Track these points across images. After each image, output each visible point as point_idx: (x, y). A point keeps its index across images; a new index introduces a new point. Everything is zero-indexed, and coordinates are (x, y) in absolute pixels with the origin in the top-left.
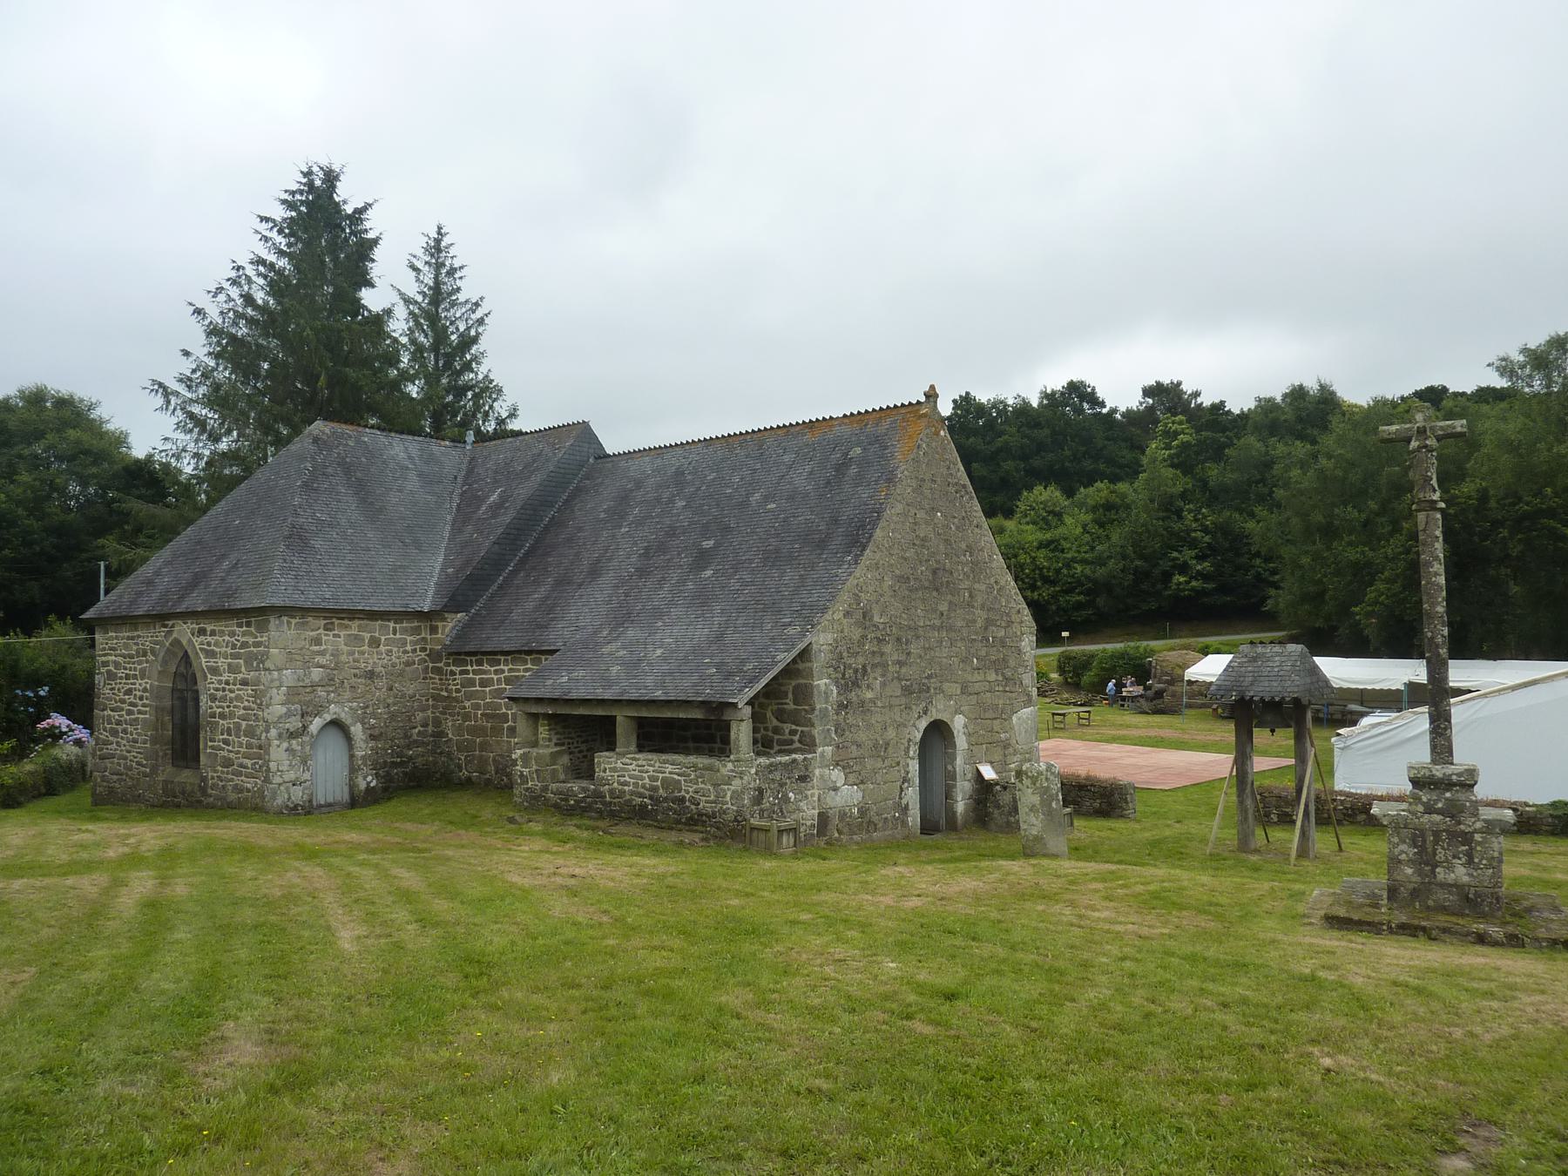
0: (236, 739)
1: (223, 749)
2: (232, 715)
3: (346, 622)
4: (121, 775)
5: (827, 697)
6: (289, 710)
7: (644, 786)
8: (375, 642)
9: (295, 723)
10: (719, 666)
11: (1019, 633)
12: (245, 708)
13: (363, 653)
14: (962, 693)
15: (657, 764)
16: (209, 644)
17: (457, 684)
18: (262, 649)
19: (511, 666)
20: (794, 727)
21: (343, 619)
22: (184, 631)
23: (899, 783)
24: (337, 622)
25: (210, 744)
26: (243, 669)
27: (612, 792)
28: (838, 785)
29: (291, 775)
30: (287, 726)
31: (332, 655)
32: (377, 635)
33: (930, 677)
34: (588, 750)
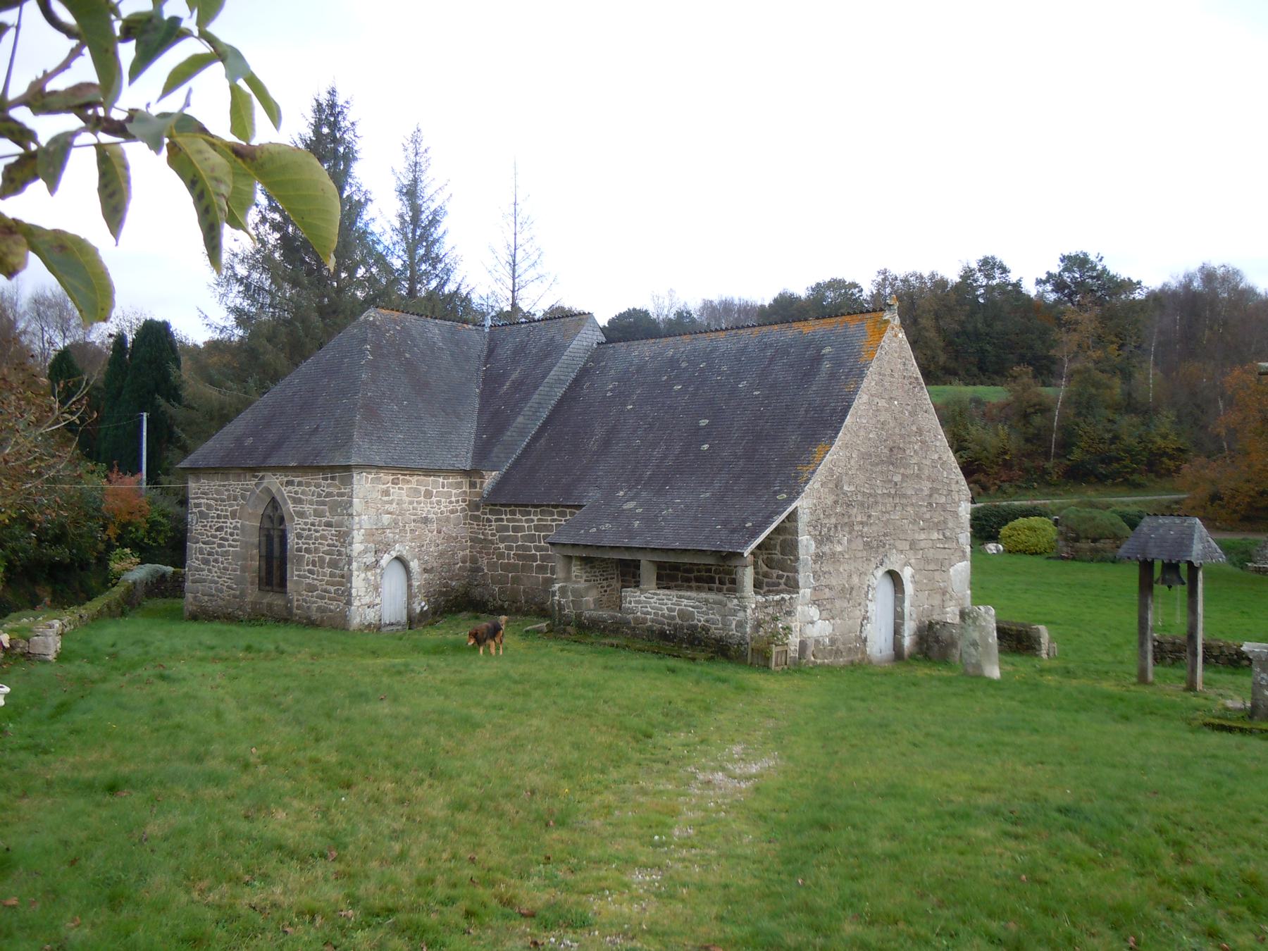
0: (320, 570)
1: (309, 578)
2: (316, 550)
3: (407, 477)
4: (213, 596)
5: (808, 550)
6: (366, 547)
7: (663, 615)
8: (428, 494)
9: (370, 559)
10: (725, 523)
11: (957, 500)
12: (328, 545)
13: (419, 503)
14: (911, 549)
15: (675, 599)
16: (296, 493)
17: (493, 529)
18: (345, 498)
19: (539, 517)
20: (781, 572)
21: (405, 475)
22: (274, 482)
23: (859, 621)
24: (401, 477)
25: (296, 573)
26: (328, 514)
27: (636, 619)
28: (815, 619)
29: (367, 600)
30: (365, 560)
31: (398, 504)
32: (430, 488)
33: (885, 535)
34: (608, 586)
